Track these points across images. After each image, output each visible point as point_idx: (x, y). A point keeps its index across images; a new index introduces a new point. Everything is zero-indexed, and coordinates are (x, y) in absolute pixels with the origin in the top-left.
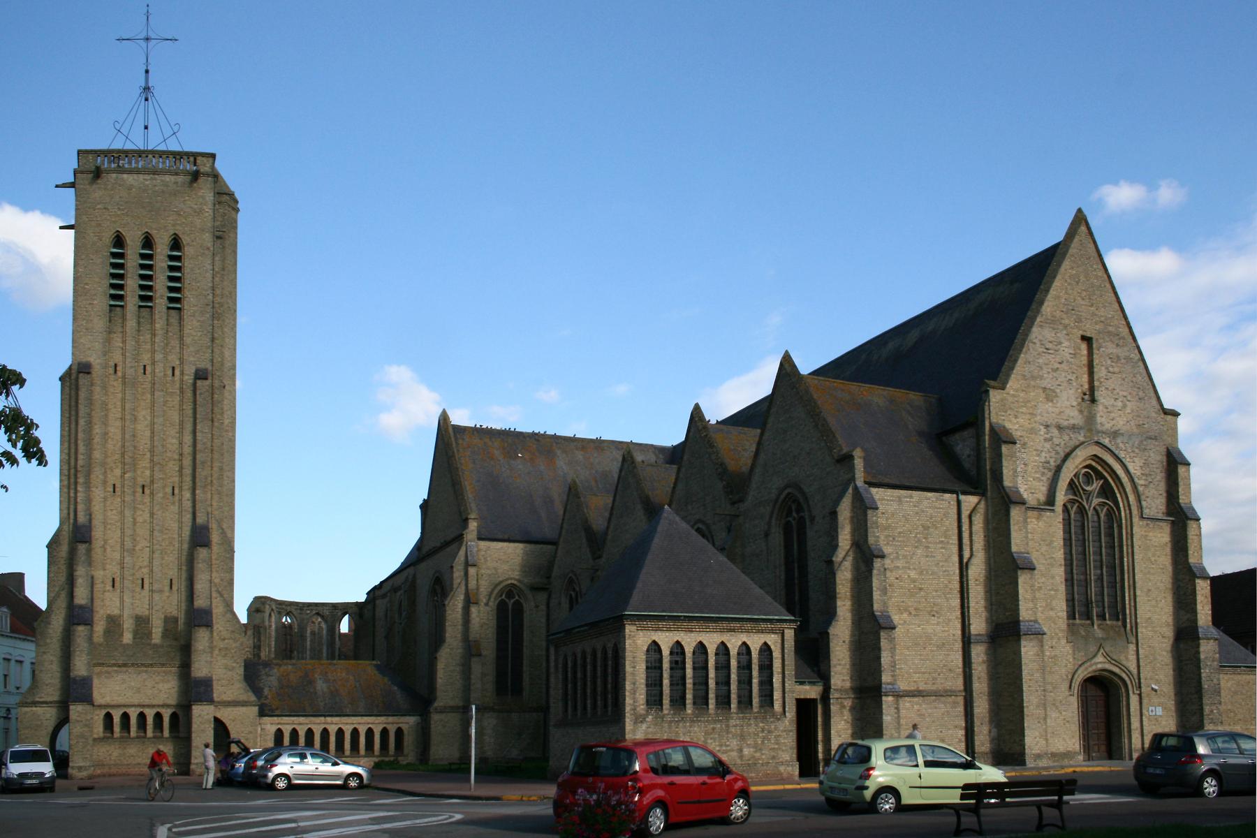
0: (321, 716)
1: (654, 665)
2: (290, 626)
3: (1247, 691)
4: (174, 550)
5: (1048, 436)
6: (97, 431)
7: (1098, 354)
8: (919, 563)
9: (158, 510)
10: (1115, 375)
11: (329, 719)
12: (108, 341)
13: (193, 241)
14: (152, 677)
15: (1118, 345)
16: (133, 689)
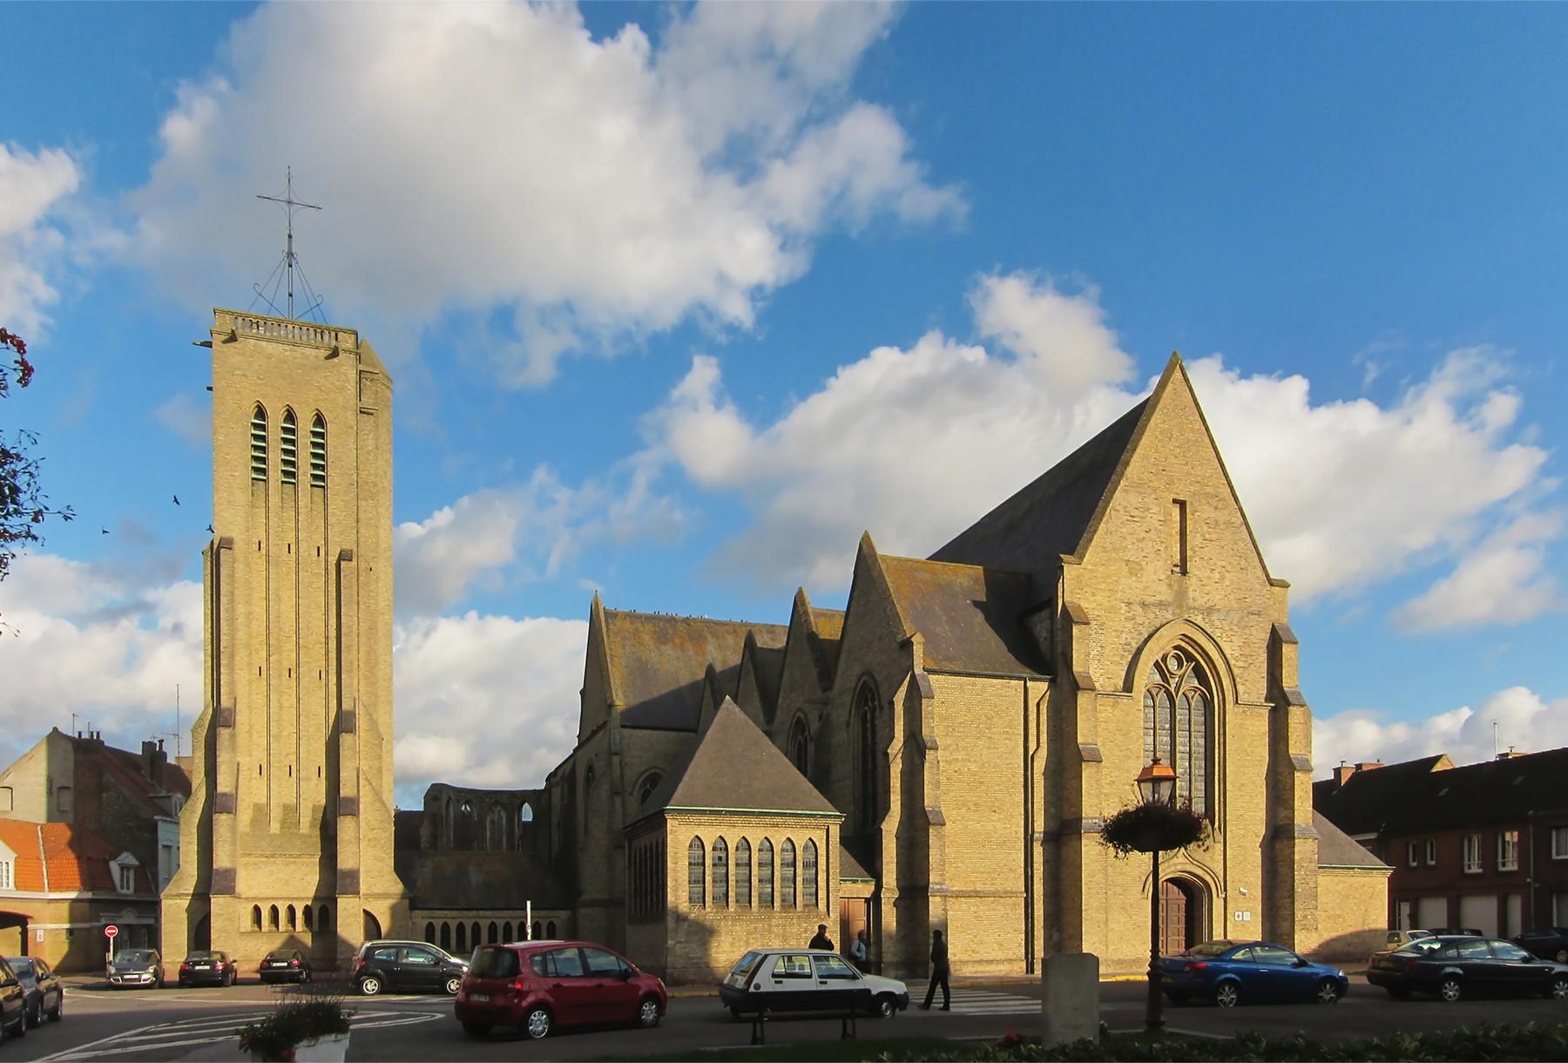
0: (474, 909)
1: (698, 864)
2: (470, 814)
3: (1361, 895)
5: (1130, 615)
6: (241, 610)
7: (1191, 519)
8: (981, 755)
9: (305, 695)
10: (1213, 543)
11: (481, 913)
15: (1216, 508)
16: (281, 880)
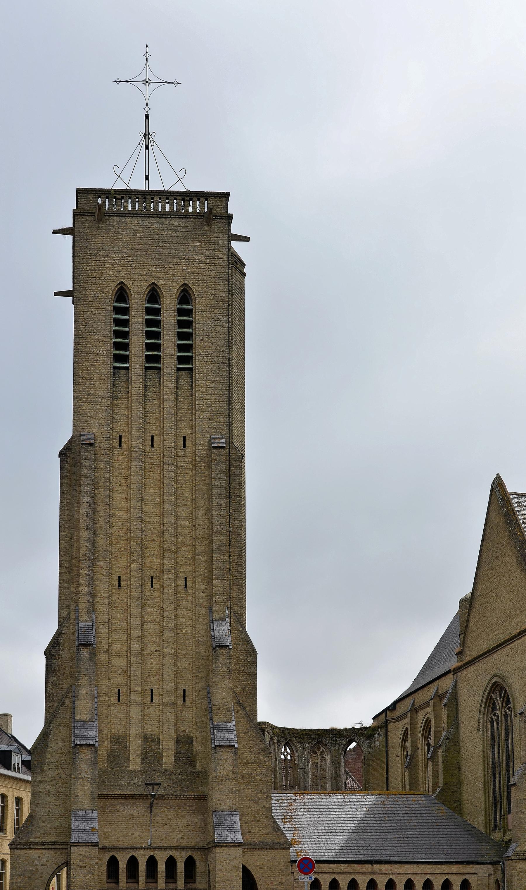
4: (187, 654)
12: (112, 407)
13: (205, 292)
14: (163, 812)
16: (141, 827)
